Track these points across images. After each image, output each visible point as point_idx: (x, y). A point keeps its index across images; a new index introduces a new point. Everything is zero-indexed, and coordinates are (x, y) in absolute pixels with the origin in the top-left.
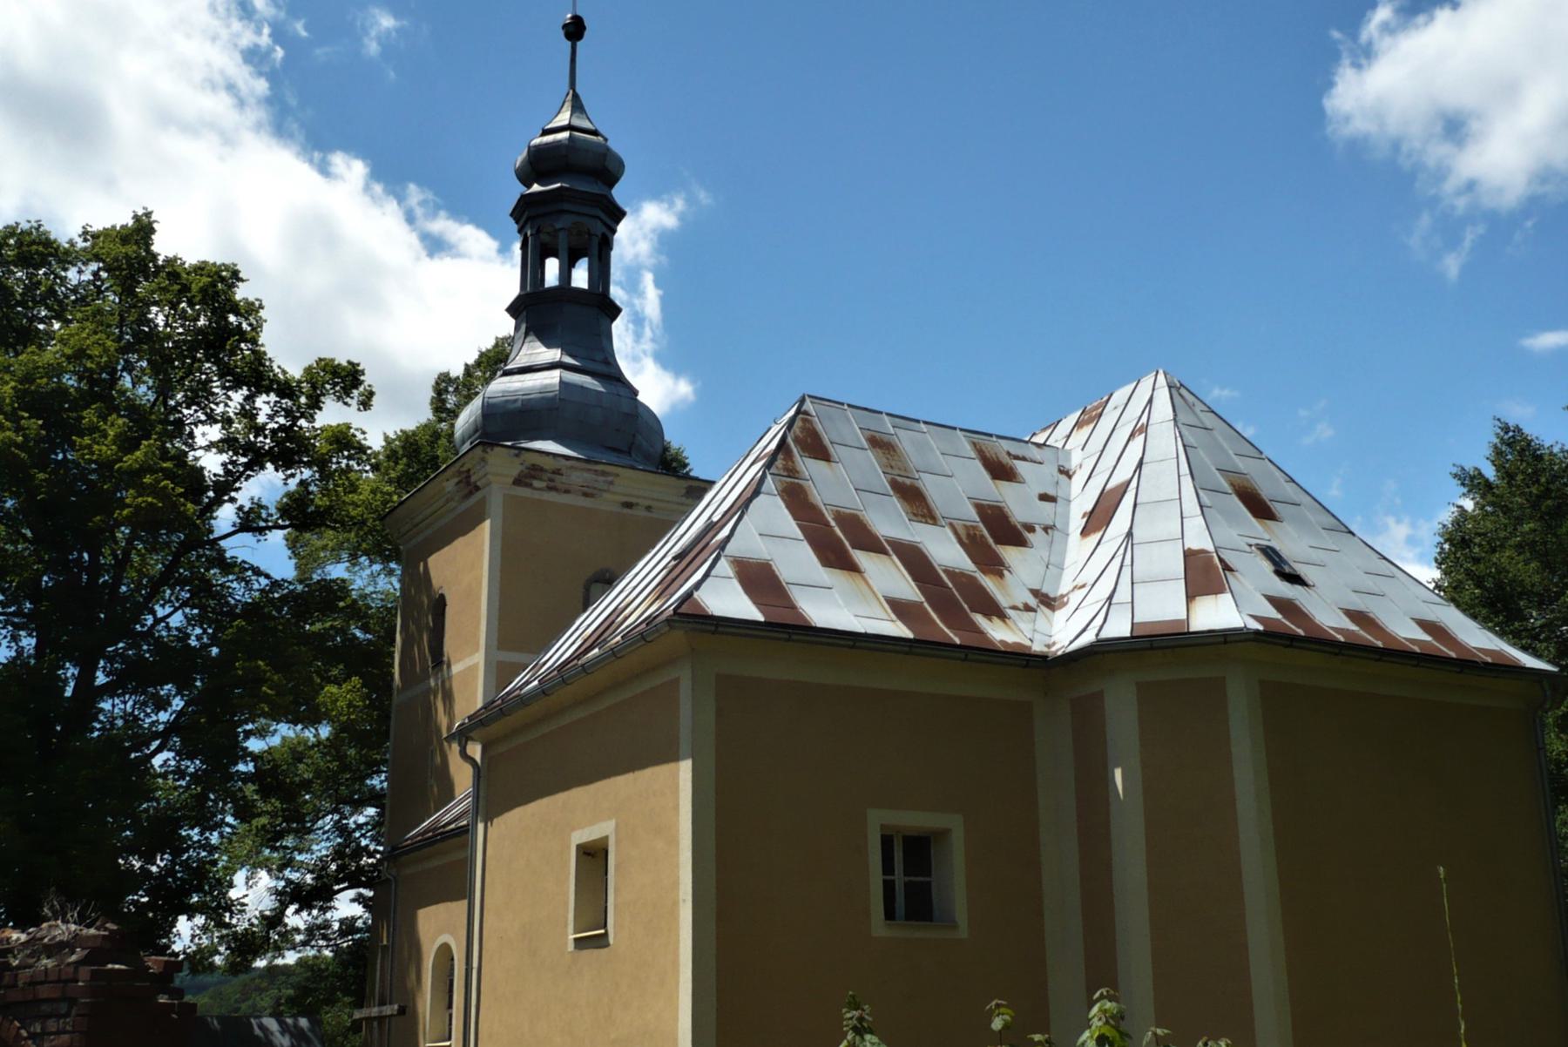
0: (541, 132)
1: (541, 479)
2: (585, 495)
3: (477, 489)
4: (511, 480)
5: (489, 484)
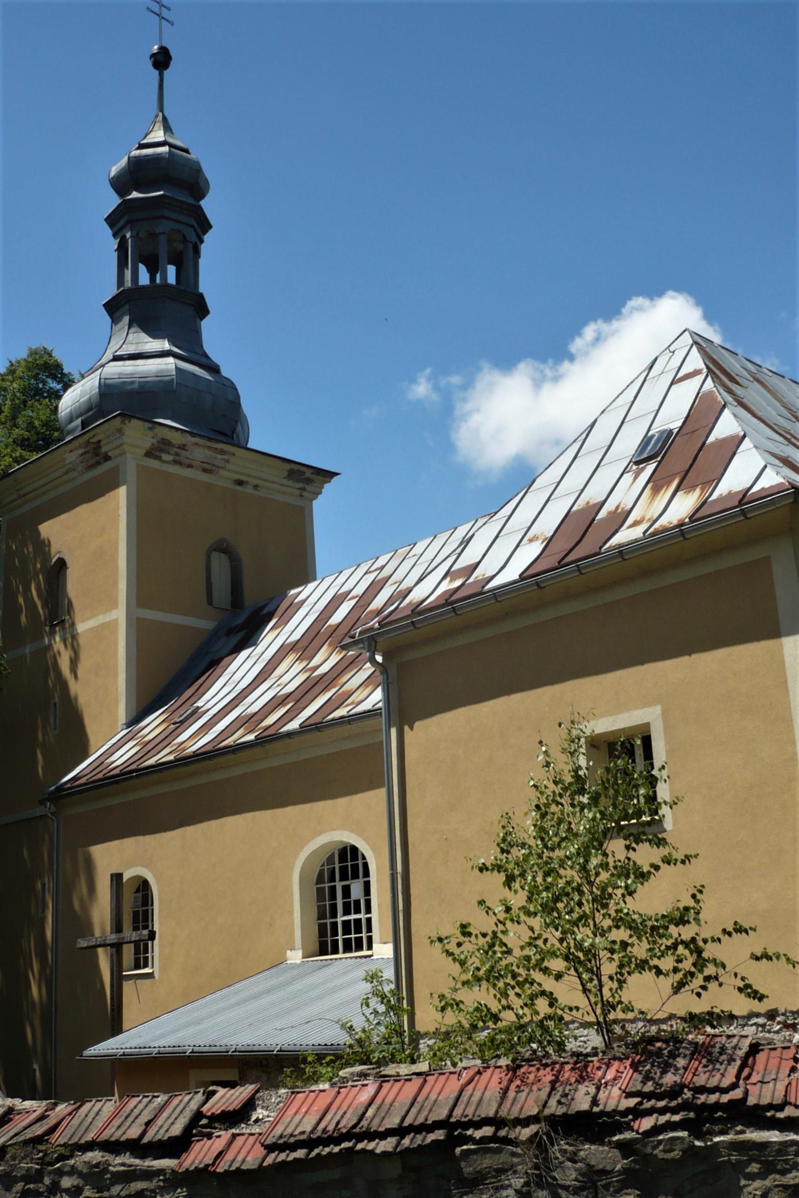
0: (137, 146)
1: (169, 453)
2: (205, 470)
3: (107, 458)
4: (144, 451)
5: (122, 454)
